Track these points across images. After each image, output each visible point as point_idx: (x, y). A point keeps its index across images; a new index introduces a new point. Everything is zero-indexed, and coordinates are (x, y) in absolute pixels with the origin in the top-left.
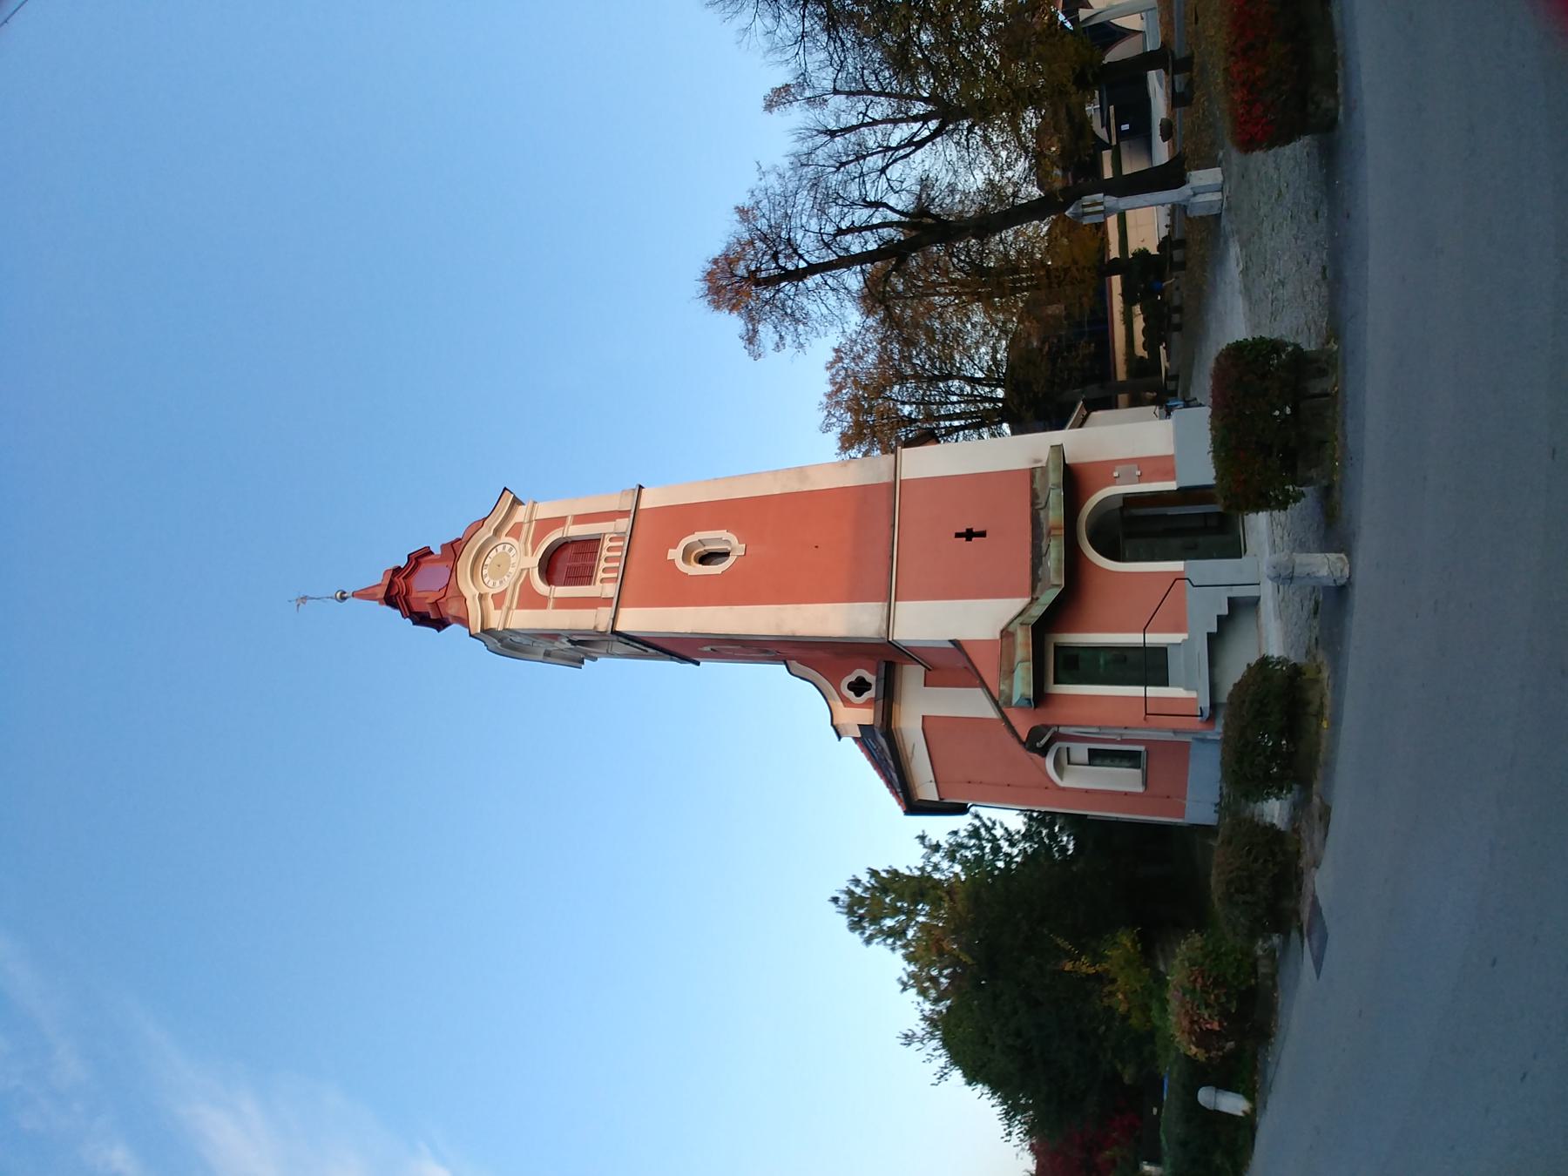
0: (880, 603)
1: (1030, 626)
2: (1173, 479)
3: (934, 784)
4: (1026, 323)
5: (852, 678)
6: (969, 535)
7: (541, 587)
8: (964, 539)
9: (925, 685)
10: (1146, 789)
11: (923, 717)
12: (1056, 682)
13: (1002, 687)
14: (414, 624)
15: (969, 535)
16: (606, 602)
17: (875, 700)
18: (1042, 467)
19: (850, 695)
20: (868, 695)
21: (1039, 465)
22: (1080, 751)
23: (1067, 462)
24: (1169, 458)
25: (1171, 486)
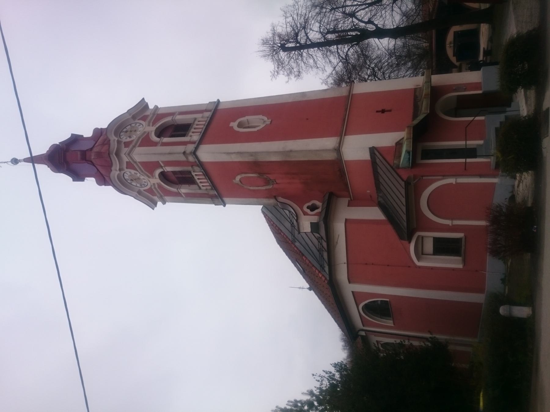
0: (336, 138)
1: (412, 127)
2: (481, 90)
3: (346, 265)
4: (366, 399)
5: (310, 204)
6: (383, 111)
7: (154, 138)
8: (381, 113)
9: (348, 206)
10: (464, 265)
11: (346, 220)
12: (422, 159)
13: (395, 162)
14: (143, 106)
15: (383, 111)
16: (194, 143)
17: (320, 213)
18: (420, 88)
19: (308, 211)
20: (316, 211)
21: (419, 87)
22: (429, 237)
23: (432, 85)
24: (480, 83)
25: (480, 92)
